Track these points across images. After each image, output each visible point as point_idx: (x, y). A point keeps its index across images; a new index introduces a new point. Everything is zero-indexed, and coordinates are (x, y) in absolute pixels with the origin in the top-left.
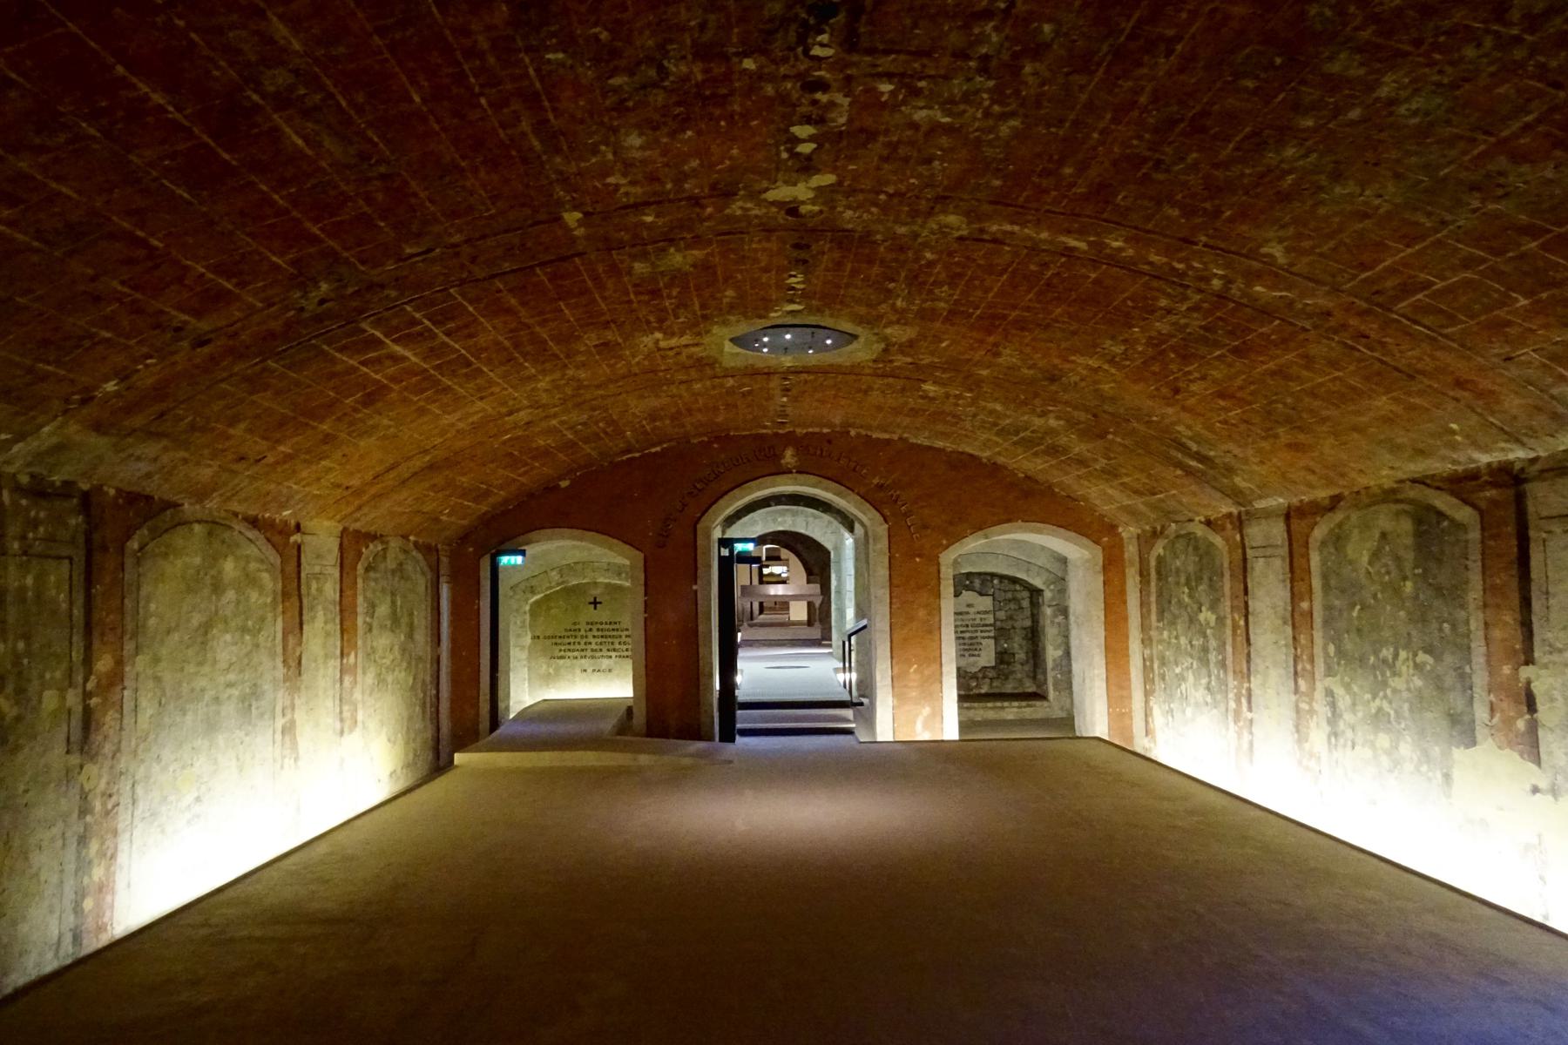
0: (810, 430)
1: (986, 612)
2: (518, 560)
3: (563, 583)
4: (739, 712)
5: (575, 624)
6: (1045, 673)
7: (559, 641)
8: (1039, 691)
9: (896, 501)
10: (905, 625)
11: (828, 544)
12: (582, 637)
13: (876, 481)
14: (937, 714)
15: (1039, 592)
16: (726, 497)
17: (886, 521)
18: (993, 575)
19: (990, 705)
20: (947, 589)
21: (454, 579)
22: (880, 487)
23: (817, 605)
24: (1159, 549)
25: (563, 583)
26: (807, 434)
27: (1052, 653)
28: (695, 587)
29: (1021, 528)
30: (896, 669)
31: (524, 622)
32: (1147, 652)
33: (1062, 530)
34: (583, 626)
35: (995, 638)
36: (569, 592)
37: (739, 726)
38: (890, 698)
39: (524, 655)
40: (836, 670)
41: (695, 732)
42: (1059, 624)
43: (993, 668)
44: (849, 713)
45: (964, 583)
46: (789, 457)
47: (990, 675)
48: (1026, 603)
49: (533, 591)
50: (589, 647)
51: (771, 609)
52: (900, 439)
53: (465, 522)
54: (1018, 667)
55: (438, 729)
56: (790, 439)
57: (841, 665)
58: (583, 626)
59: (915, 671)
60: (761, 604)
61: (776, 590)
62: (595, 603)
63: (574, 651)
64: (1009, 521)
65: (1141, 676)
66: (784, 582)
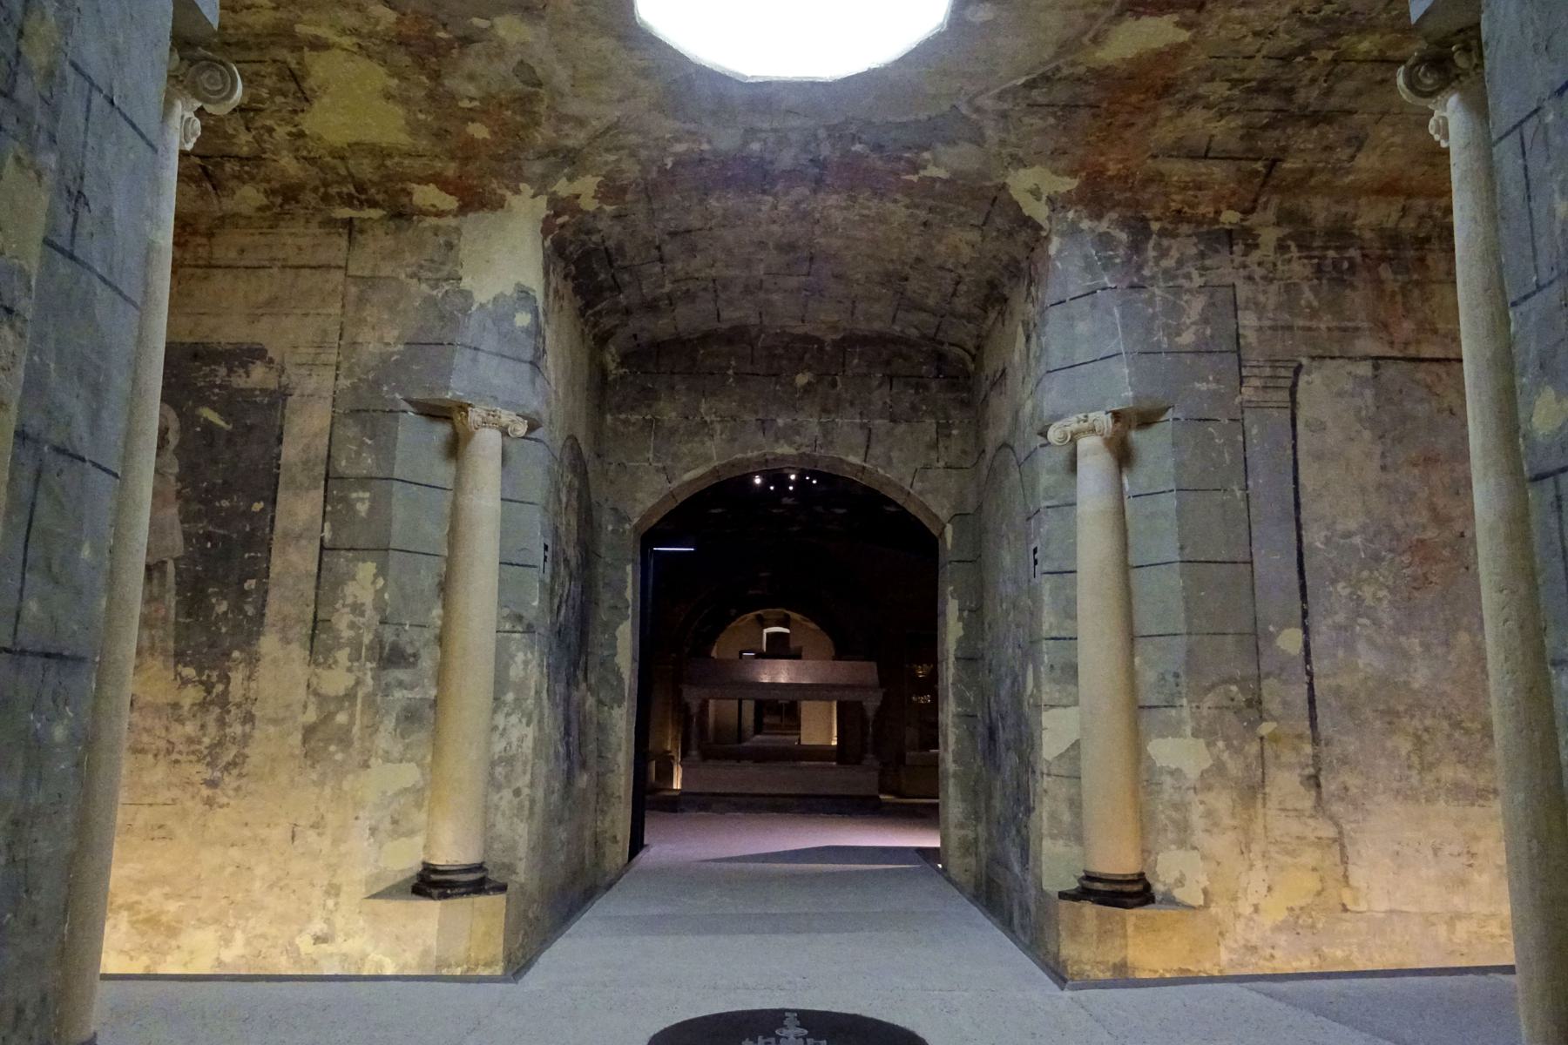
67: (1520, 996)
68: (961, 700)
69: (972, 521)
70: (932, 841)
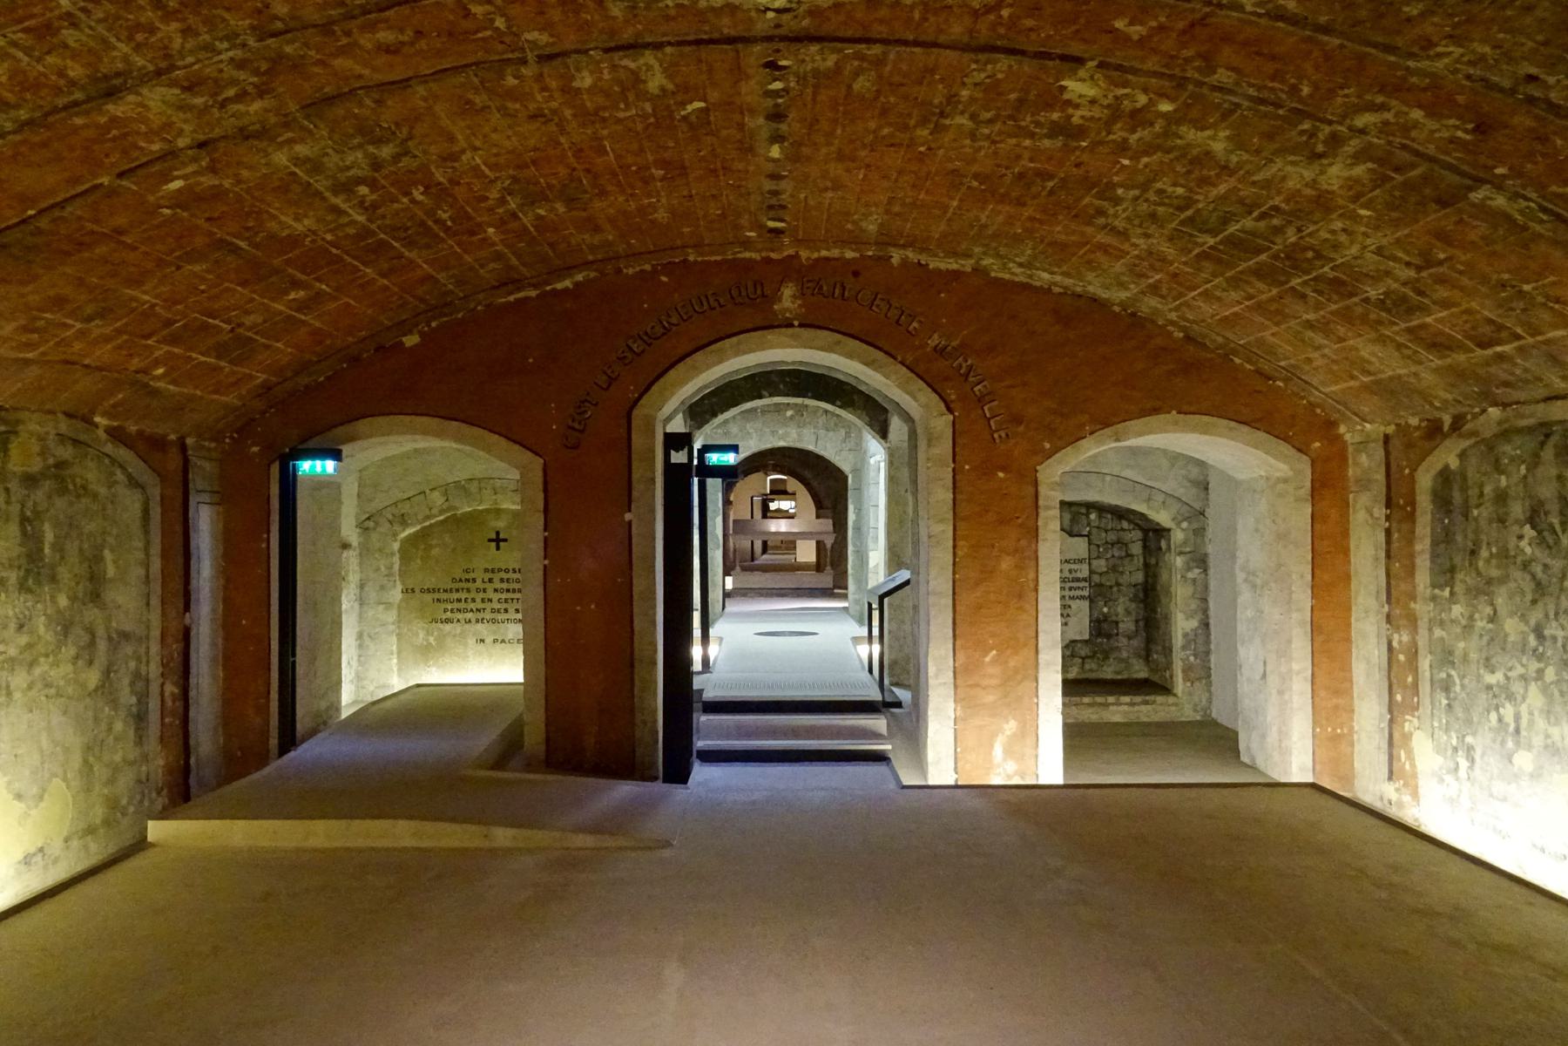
0: (824, 253)
1: (1081, 561)
2: (329, 466)
3: (449, 509)
4: (702, 720)
5: (467, 571)
6: (1168, 651)
7: (444, 596)
8: (1155, 678)
9: (967, 375)
10: (977, 584)
11: (843, 462)
12: (478, 590)
13: (934, 340)
14: (1029, 731)
15: (1160, 532)
16: (681, 366)
17: (950, 410)
18: (1090, 506)
19: (1086, 700)
20: (1050, 523)
21: (225, 497)
22: (940, 351)
23: (829, 546)
24: (1448, 455)
25: (449, 509)
26: (817, 260)
27: (1182, 624)
28: (628, 516)
29: (1176, 423)
30: (961, 656)
31: (390, 567)
32: (1401, 638)
33: (1245, 429)
34: (479, 575)
35: (1091, 600)
36: (456, 523)
37: (700, 744)
38: (952, 705)
39: (392, 616)
40: (856, 640)
41: (625, 766)
42: (1194, 580)
43: (1086, 642)
44: (879, 723)
45: (1076, 514)
46: (788, 300)
47: (1083, 653)
48: (1136, 549)
49: (403, 521)
50: (488, 606)
51: (776, 548)
52: (975, 270)
53: (230, 399)
54: (1123, 641)
55: (186, 750)
56: (790, 269)
57: (864, 631)
58: (479, 575)
59: (994, 661)
60: (765, 544)
61: (779, 526)
62: (498, 540)
63: (466, 611)
64: (1155, 411)
65: (1379, 677)
66: (792, 517)
67: (349, 530)
68: (854, 545)
69: (858, 471)
70: (845, 604)
